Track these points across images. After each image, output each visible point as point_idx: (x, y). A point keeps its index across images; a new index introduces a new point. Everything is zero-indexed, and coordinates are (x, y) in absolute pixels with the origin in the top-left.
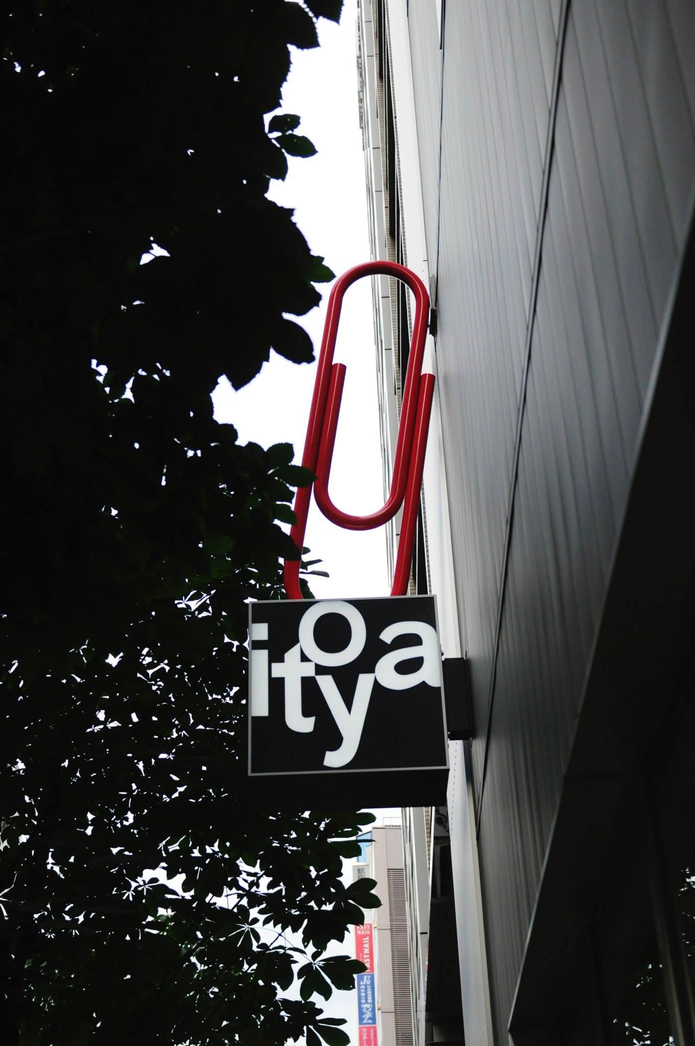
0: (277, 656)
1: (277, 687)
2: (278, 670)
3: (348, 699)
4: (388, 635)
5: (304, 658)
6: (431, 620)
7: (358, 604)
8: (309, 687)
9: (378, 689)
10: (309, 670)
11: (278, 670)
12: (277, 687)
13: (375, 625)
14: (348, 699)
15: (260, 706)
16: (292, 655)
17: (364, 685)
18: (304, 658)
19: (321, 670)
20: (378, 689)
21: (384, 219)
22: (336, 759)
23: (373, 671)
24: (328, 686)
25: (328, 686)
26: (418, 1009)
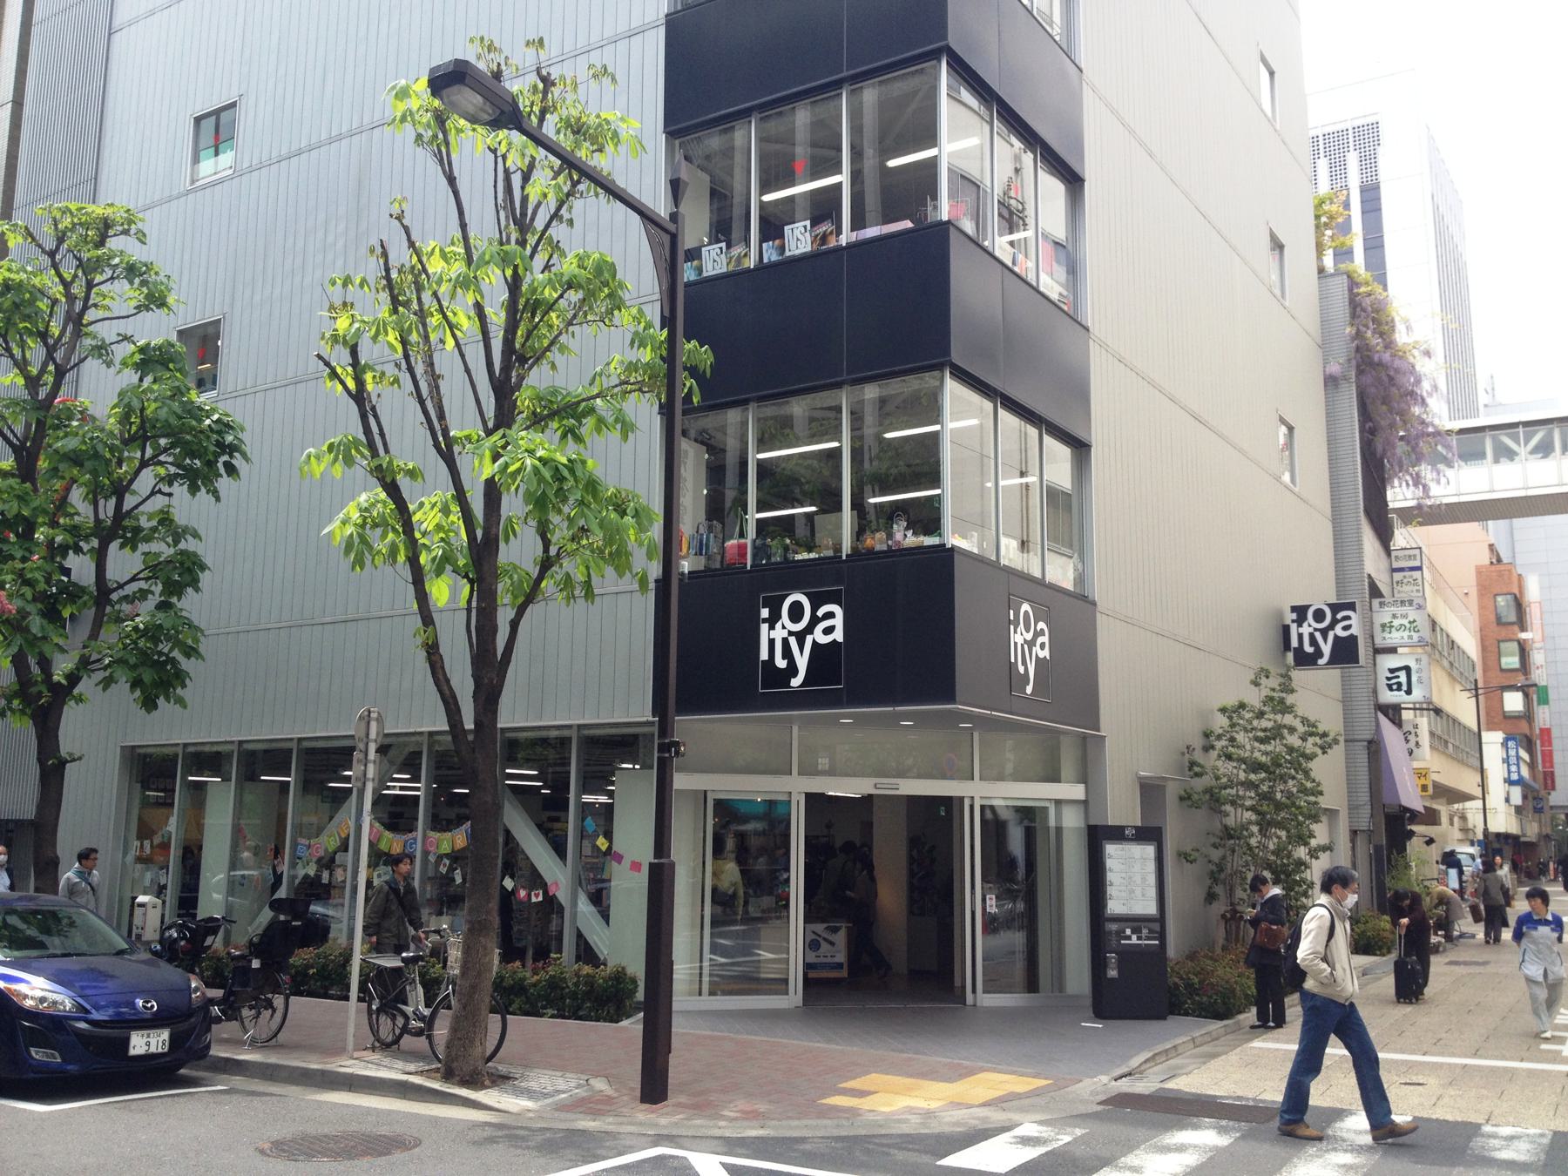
0: (1300, 625)
1: (1300, 636)
2: (1301, 630)
3: (1325, 639)
4: (1339, 616)
5: (784, 627)
6: (1354, 610)
7: (1329, 605)
8: (1312, 636)
9: (1336, 637)
10: (1311, 630)
11: (1301, 630)
12: (1300, 636)
13: (1334, 613)
14: (1325, 639)
15: (764, 655)
16: (1305, 624)
17: (809, 640)
18: (1310, 626)
19: (1316, 630)
20: (1336, 637)
21: (658, 466)
22: (796, 682)
23: (812, 633)
24: (1318, 635)
25: (1318, 635)
26: (1487, 807)
